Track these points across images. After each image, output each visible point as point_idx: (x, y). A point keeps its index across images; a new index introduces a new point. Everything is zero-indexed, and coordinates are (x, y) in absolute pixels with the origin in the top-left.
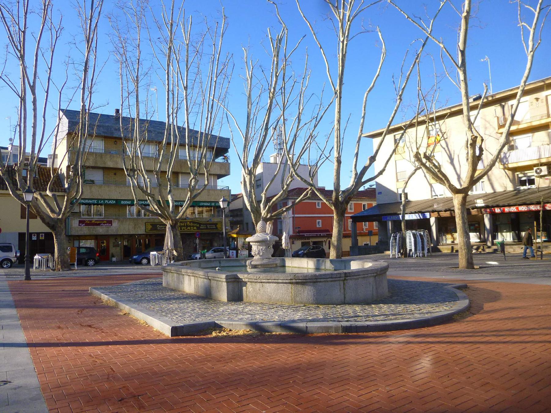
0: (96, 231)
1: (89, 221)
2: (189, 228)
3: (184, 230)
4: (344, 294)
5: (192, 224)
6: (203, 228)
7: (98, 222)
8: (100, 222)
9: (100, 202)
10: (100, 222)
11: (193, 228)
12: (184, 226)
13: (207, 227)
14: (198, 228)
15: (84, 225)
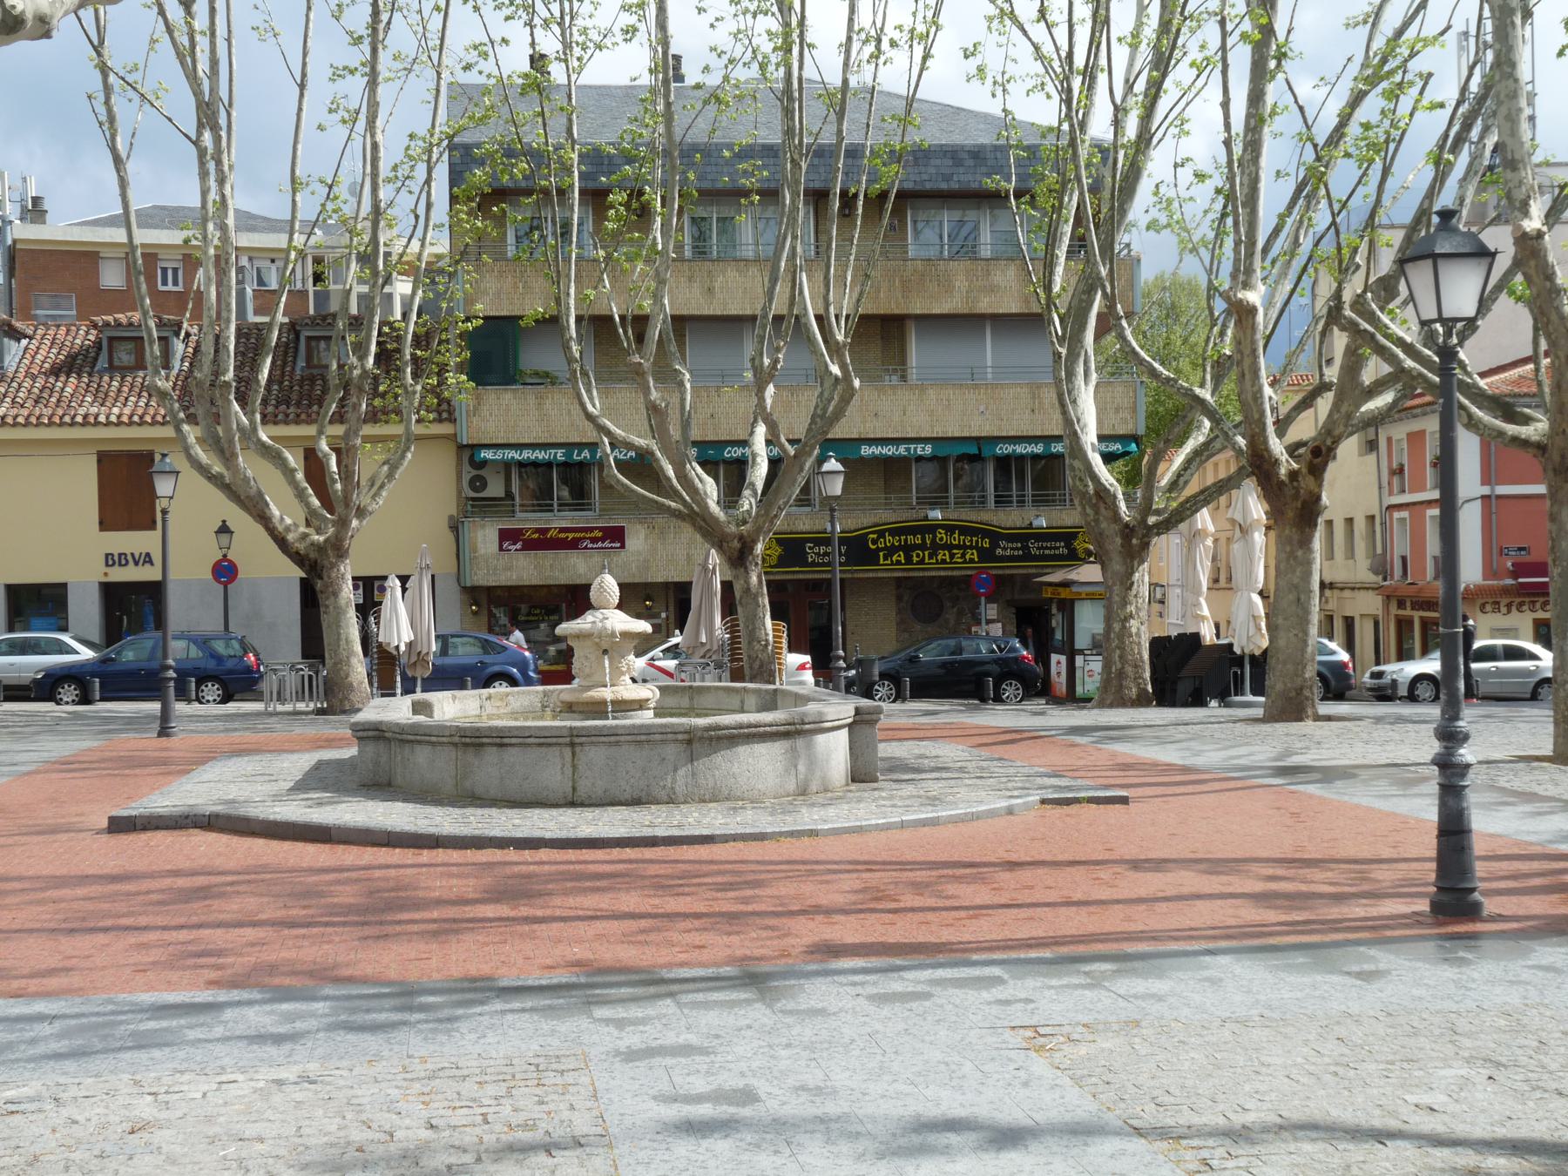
0: (562, 570)
1: (537, 530)
2: (943, 555)
3: (922, 562)
4: (574, 781)
5: (956, 538)
6: (1008, 553)
7: (571, 536)
8: (578, 535)
9: (578, 455)
10: (578, 535)
11: (963, 555)
12: (923, 547)
13: (1025, 548)
14: (987, 555)
15: (519, 546)
